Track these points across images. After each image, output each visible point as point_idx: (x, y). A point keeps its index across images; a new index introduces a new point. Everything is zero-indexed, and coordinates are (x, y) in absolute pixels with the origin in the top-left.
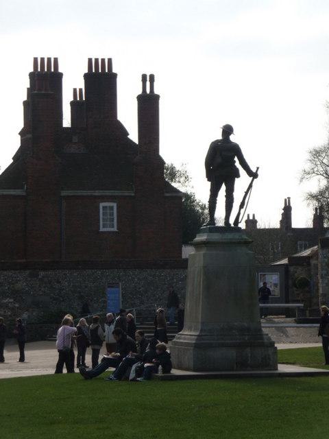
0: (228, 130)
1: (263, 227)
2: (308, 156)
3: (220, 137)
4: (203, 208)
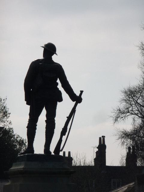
0: (50, 49)
1: (78, 165)
2: (122, 96)
3: (41, 57)
4: (21, 143)
